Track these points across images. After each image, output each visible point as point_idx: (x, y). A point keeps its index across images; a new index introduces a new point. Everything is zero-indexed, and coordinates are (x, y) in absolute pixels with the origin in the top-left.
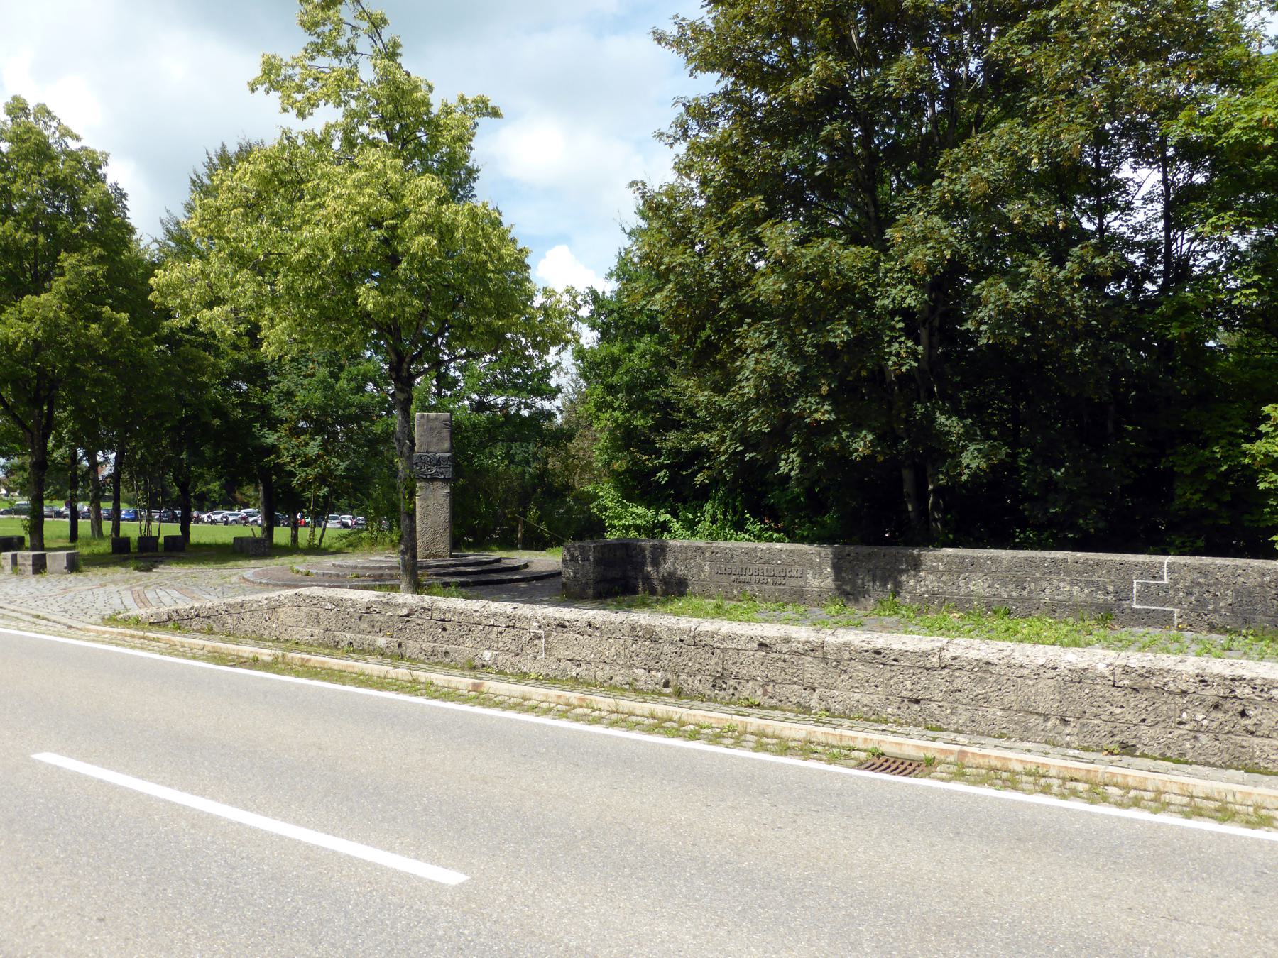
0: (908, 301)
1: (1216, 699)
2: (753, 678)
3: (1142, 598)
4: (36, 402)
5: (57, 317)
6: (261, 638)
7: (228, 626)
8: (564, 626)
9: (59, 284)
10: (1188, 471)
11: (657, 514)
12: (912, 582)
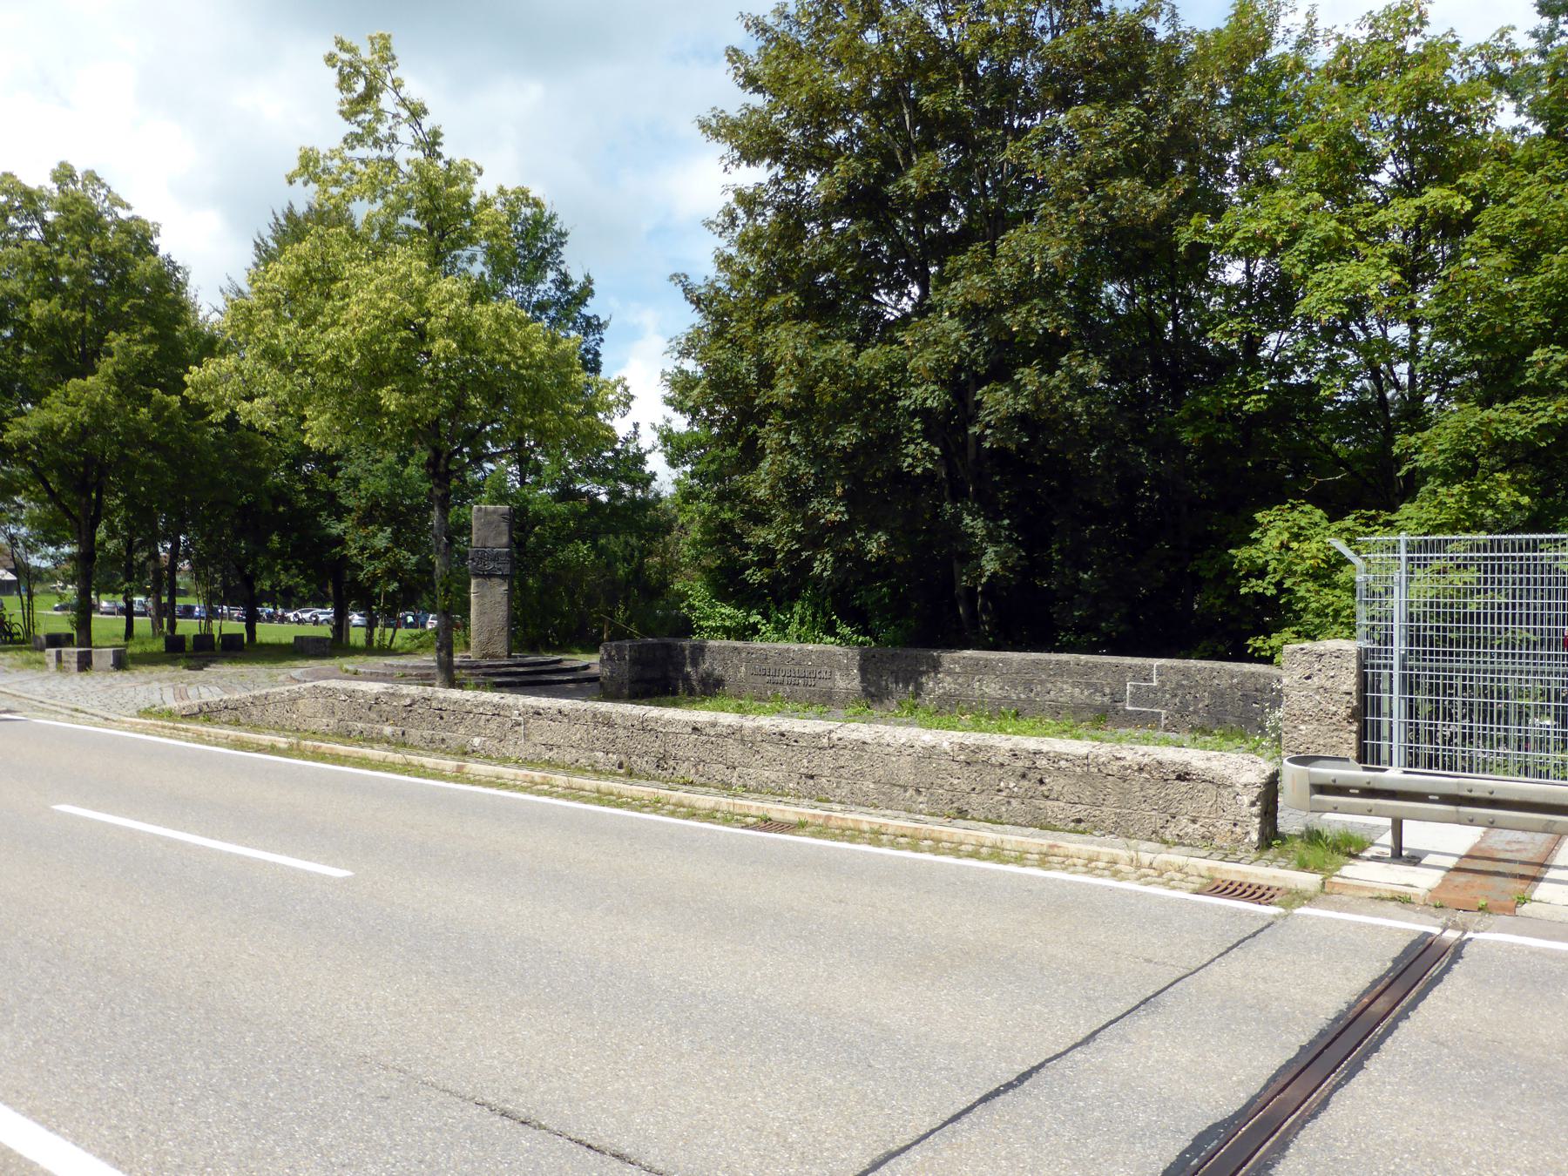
0: (929, 402)
1: (1023, 770)
2: (688, 759)
3: (1135, 700)
4: (83, 487)
5: (104, 401)
6: (283, 728)
7: (254, 717)
8: (539, 714)
9: (106, 365)
10: (1211, 576)
11: (748, 615)
12: (931, 684)
